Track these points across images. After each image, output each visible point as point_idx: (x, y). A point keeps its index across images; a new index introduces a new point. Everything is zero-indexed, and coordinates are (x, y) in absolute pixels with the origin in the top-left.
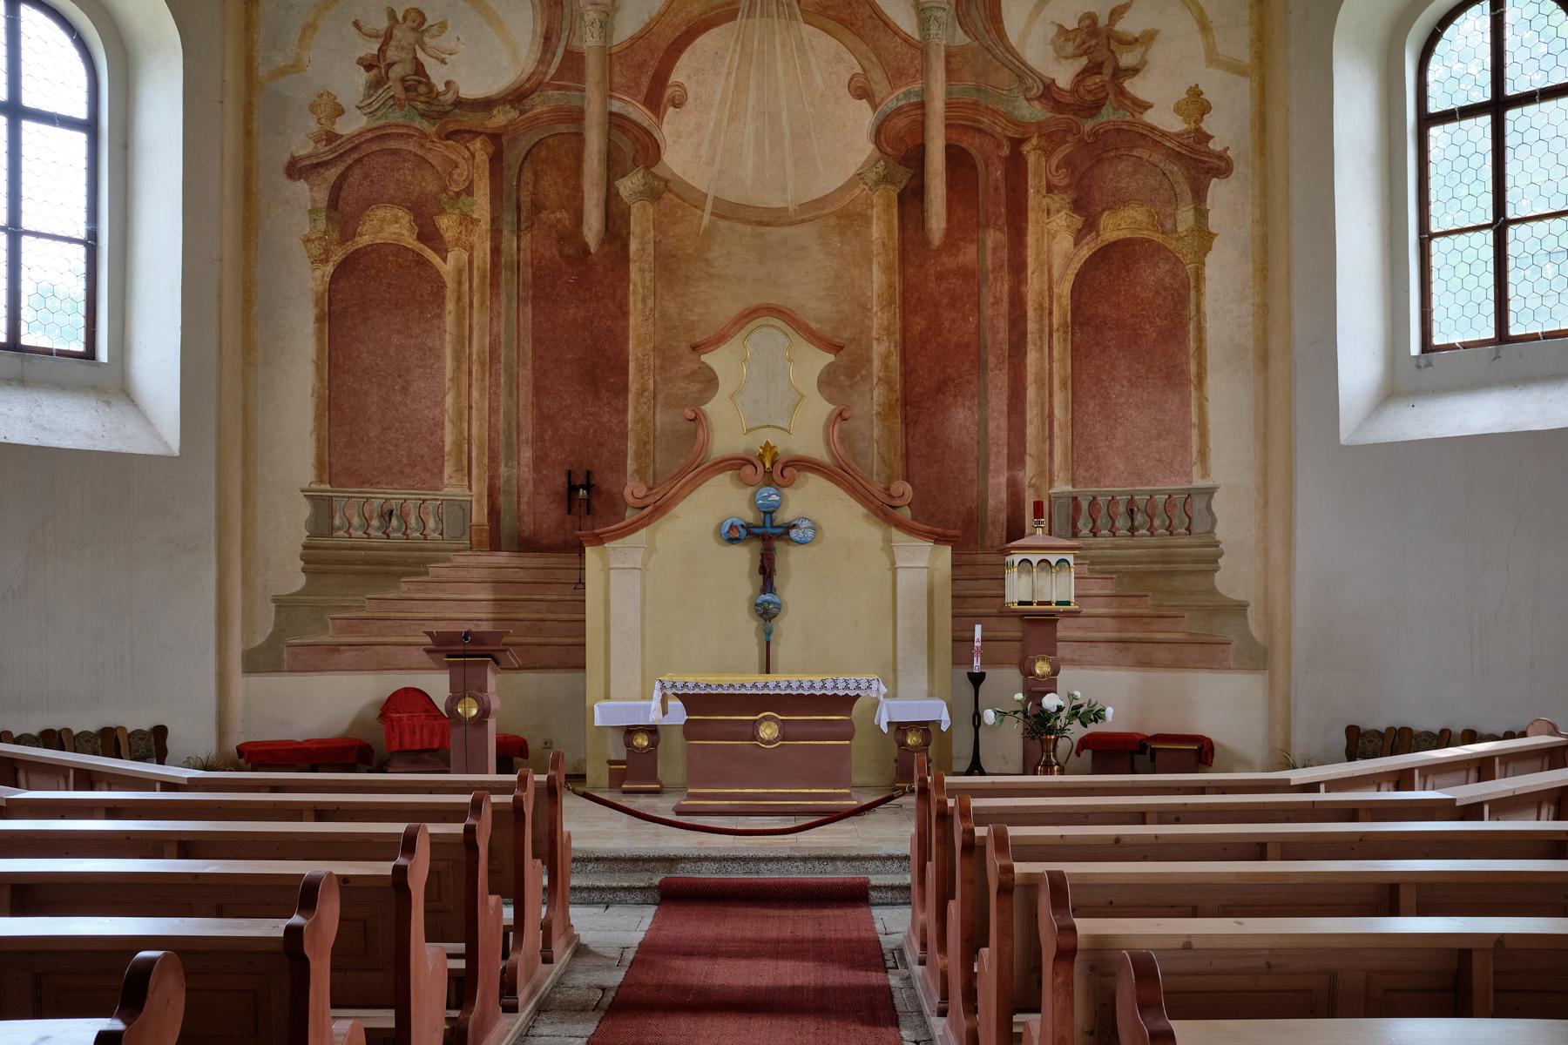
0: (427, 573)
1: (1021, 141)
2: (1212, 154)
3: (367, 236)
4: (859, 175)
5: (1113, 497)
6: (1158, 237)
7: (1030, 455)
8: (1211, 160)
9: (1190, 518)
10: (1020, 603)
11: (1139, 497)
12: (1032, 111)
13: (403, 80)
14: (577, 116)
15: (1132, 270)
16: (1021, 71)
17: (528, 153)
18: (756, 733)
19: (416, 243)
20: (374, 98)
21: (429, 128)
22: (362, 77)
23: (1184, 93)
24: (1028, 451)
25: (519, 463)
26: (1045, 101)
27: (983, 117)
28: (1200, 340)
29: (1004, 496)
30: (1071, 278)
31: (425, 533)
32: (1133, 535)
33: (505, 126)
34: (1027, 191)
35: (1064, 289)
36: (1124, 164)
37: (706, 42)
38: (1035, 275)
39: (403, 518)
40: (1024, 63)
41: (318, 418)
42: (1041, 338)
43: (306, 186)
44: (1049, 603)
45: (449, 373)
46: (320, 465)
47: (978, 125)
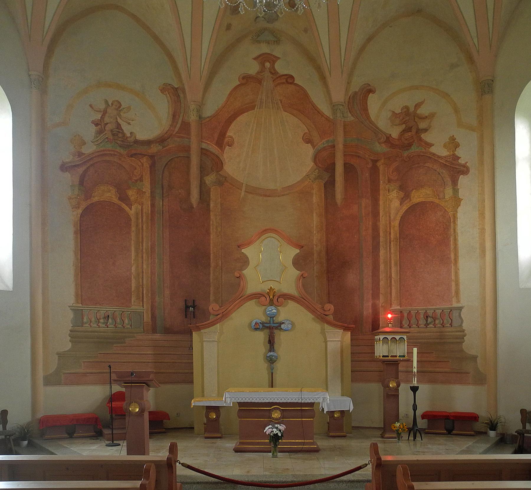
0: (125, 343)
1: (377, 161)
2: (460, 165)
3: (96, 198)
4: (307, 175)
5: (418, 311)
6: (437, 201)
7: (382, 294)
8: (460, 167)
9: (451, 320)
10: (383, 356)
11: (429, 311)
12: (381, 148)
13: (112, 131)
14: (187, 149)
15: (425, 215)
16: (376, 131)
17: (166, 164)
18: (270, 415)
19: (118, 201)
20: (99, 138)
21: (122, 151)
22: (93, 129)
23: (448, 139)
24: (381, 292)
25: (164, 296)
26: (387, 144)
27: (360, 151)
28: (456, 244)
30: (399, 218)
31: (124, 325)
32: (427, 327)
33: (156, 152)
34: (379, 182)
35: (396, 223)
36: (421, 170)
37: (242, 118)
38: (383, 218)
39: (114, 319)
40: (378, 128)
41: (76, 275)
43: (69, 175)
44: (396, 356)
45: (133, 258)
46: (77, 295)
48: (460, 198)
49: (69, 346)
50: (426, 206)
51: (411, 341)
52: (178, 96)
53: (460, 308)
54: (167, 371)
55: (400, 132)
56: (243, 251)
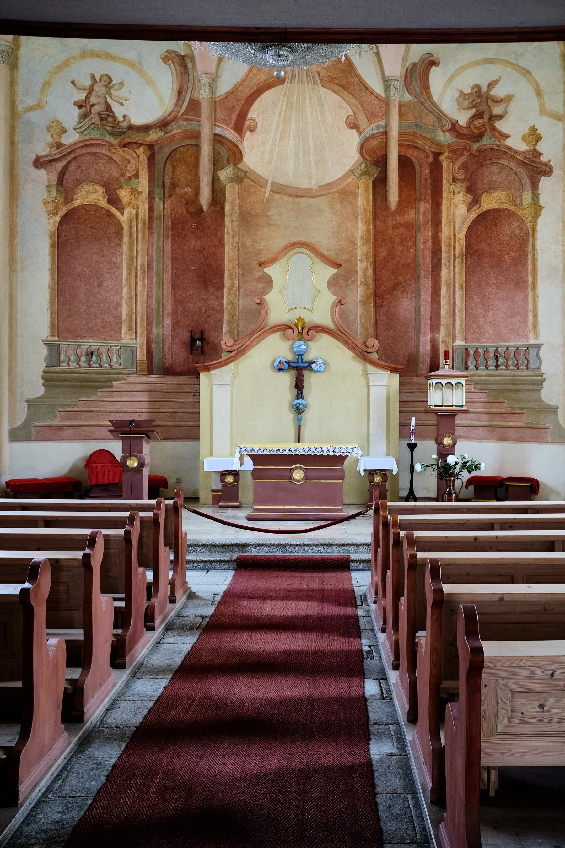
0: (112, 387)
2: (541, 163)
3: (79, 200)
4: (351, 171)
5: (487, 348)
6: (512, 208)
7: (443, 325)
8: (541, 166)
9: (528, 361)
10: (436, 406)
12: (445, 138)
13: (99, 114)
14: (196, 135)
16: (439, 116)
17: (169, 155)
20: (83, 124)
21: (112, 140)
22: (76, 112)
24: (441, 323)
25: (163, 326)
27: (419, 140)
29: (428, 347)
30: (465, 229)
31: (111, 364)
32: (497, 369)
34: (442, 181)
35: (462, 235)
36: (494, 168)
37: (268, 96)
38: (446, 227)
39: (99, 356)
40: (441, 111)
41: (52, 301)
42: (449, 261)
44: (451, 406)
47: (418, 146)
48: (541, 205)
49: (41, 391)
50: (499, 215)
51: (478, 386)
52: (185, 66)
53: (538, 346)
54: (166, 423)
55: (469, 118)
56: (265, 270)
